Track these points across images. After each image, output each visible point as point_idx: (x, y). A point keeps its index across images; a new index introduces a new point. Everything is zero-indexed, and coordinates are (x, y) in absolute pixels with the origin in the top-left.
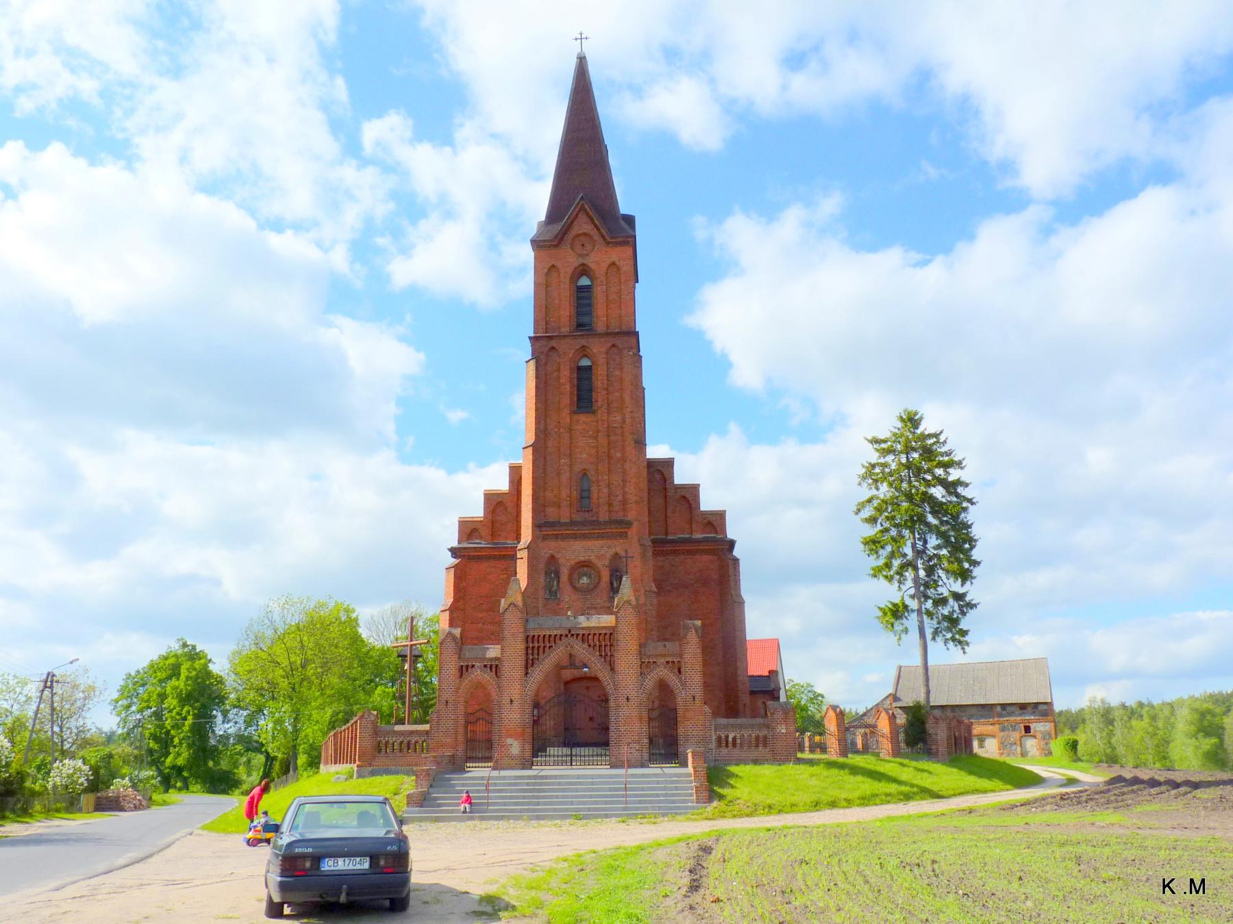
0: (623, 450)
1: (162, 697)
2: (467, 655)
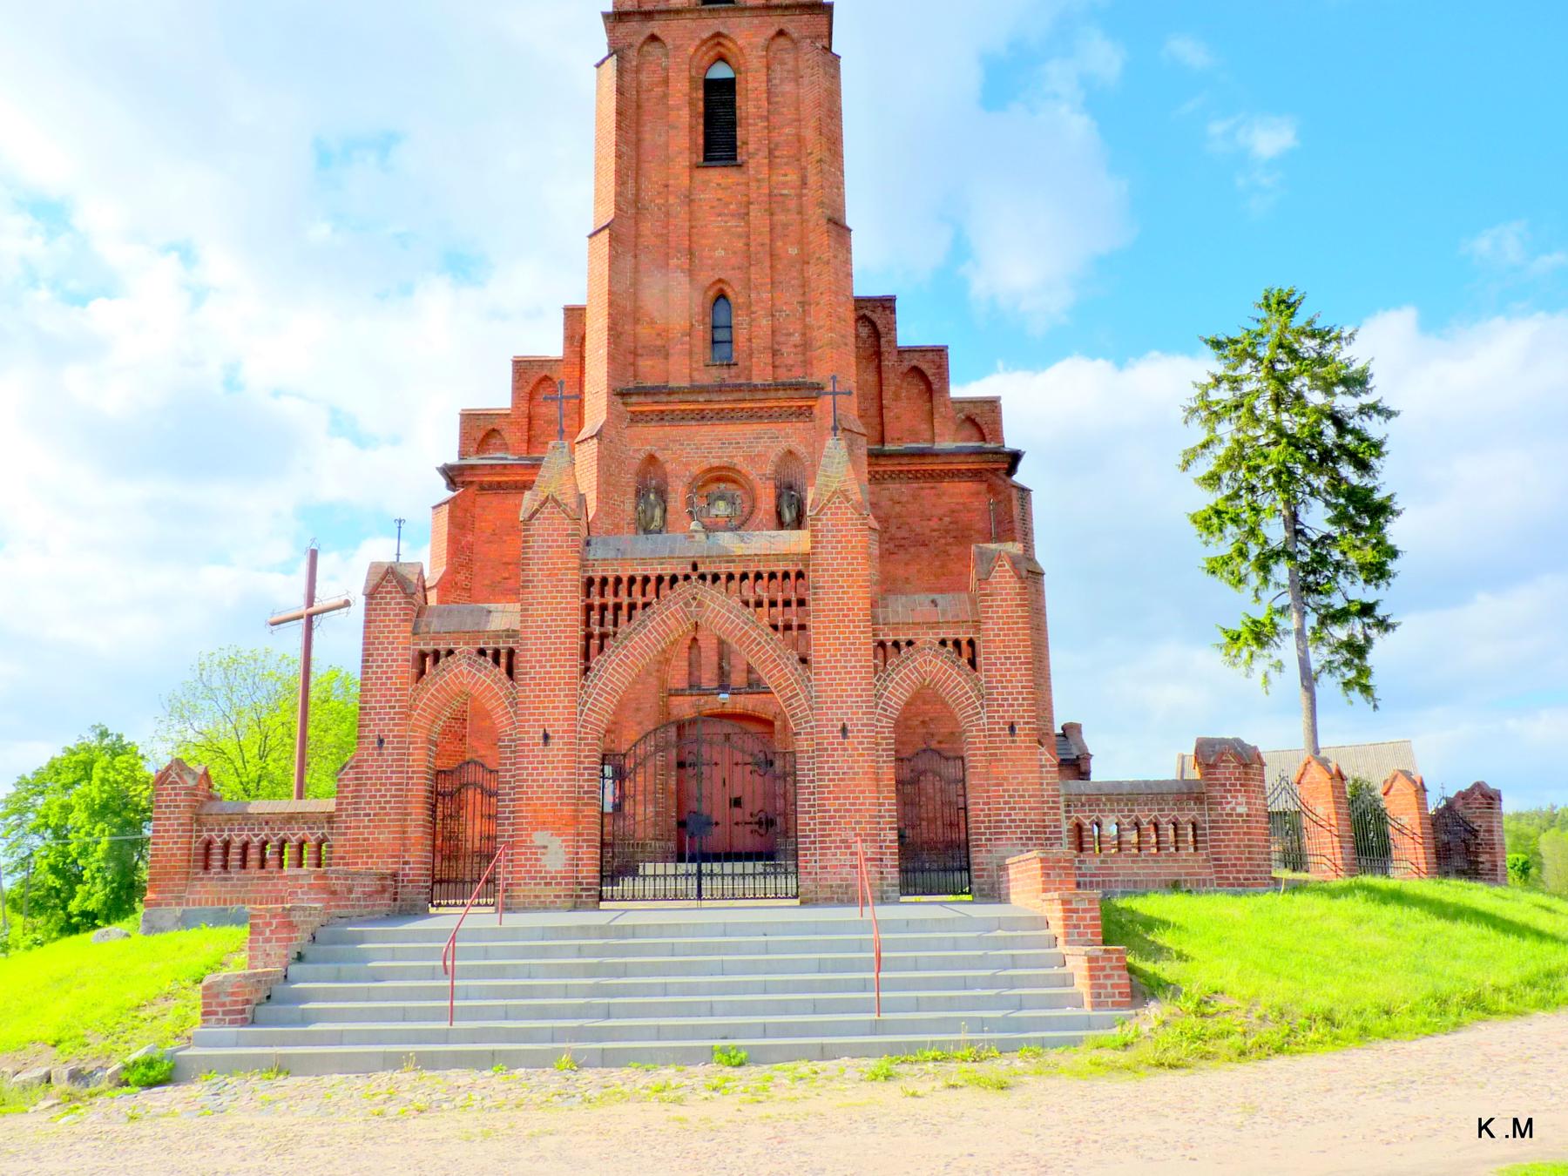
0: (802, 242)
1: (67, 809)
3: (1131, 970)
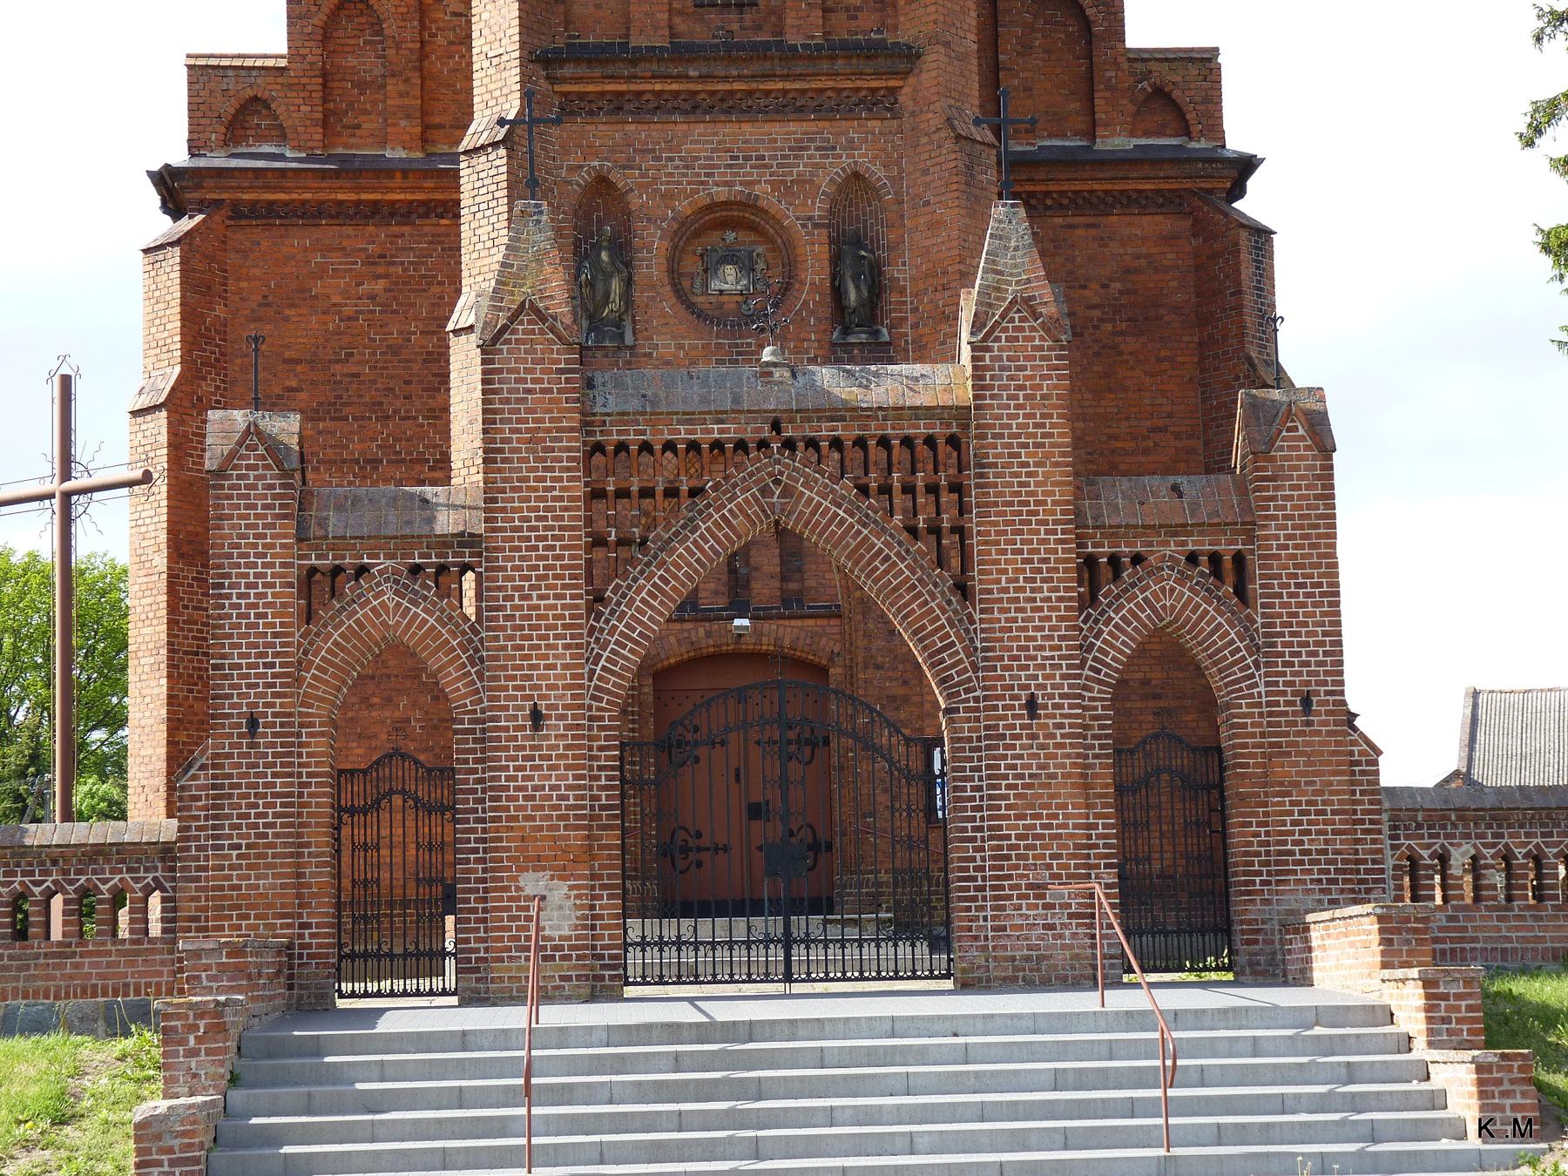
2: (335, 525)
3: (1541, 1087)
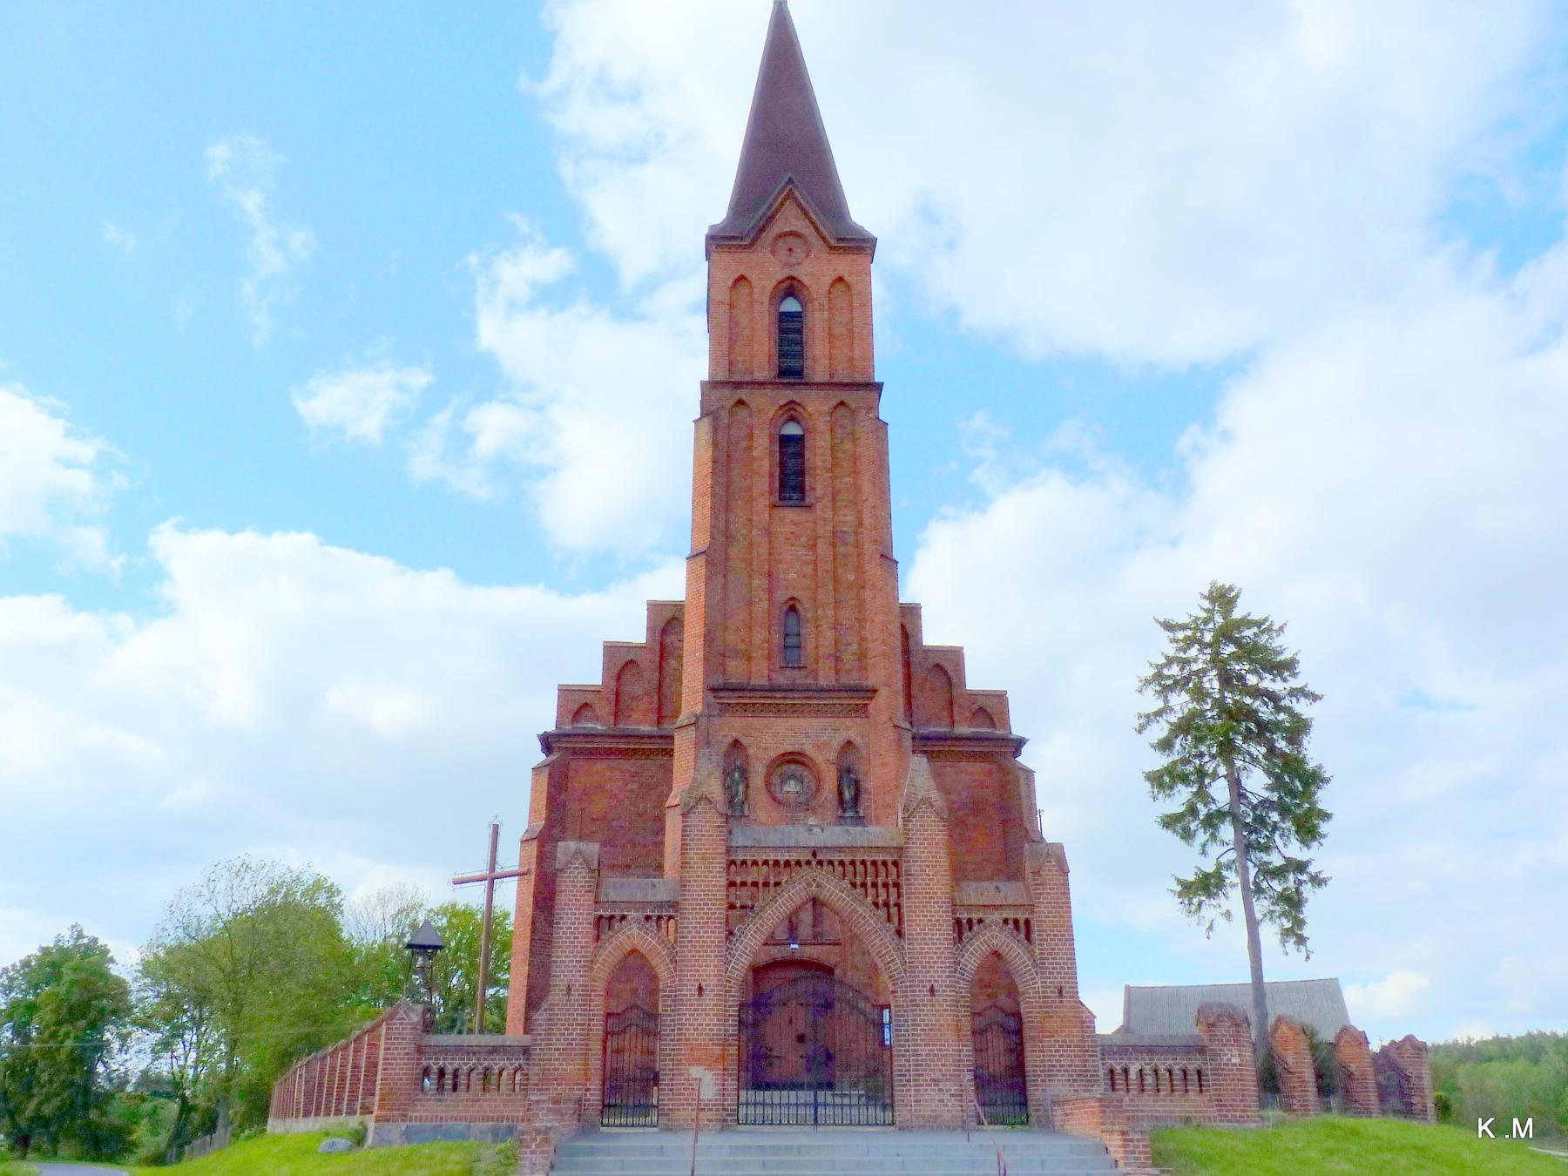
0: (859, 570)
2: (612, 896)
